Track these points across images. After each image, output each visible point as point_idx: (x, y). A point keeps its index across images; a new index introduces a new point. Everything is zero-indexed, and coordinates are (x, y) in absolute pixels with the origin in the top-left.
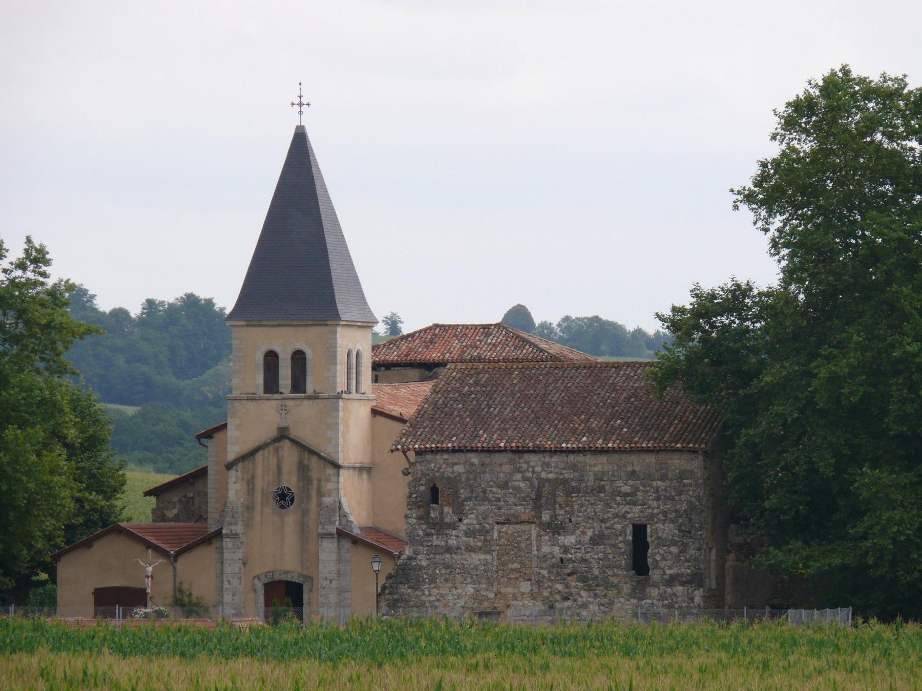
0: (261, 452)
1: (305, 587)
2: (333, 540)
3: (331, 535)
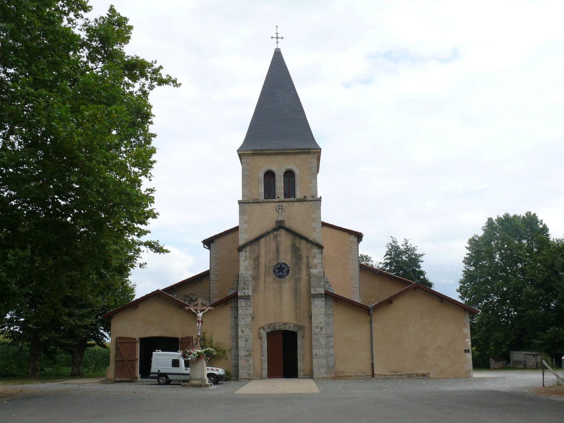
0: (264, 239)
1: (298, 334)
2: (322, 299)
3: (321, 294)
